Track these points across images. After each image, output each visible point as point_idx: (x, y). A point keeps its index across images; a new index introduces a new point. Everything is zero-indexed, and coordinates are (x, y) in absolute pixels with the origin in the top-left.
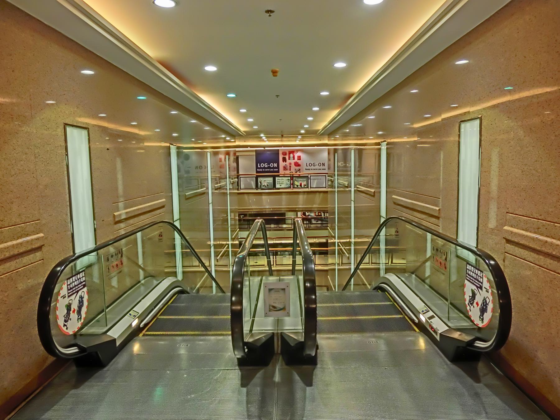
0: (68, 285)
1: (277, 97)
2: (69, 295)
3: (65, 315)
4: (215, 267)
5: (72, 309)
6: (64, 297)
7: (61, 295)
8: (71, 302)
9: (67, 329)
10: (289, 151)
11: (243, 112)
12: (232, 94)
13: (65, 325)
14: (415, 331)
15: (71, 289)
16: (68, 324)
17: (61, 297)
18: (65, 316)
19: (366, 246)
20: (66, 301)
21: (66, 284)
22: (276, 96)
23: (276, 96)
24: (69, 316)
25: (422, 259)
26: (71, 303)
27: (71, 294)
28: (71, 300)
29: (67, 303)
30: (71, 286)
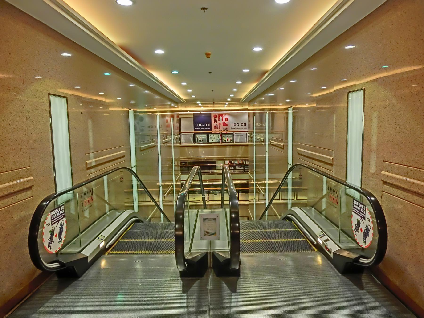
0: (51, 216)
1: (210, 74)
2: (52, 223)
3: (49, 238)
5: (55, 234)
6: (48, 225)
7: (46, 224)
8: (53, 228)
9: (51, 249)
10: (219, 115)
11: (184, 85)
12: (176, 71)
13: (49, 246)
15: (54, 218)
16: (52, 245)
17: (46, 225)
18: (49, 239)
20: (50, 228)
21: (50, 215)
22: (209, 73)
23: (209, 73)
24: (53, 240)
26: (54, 229)
27: (53, 222)
28: (54, 227)
29: (51, 229)
30: (54, 217)
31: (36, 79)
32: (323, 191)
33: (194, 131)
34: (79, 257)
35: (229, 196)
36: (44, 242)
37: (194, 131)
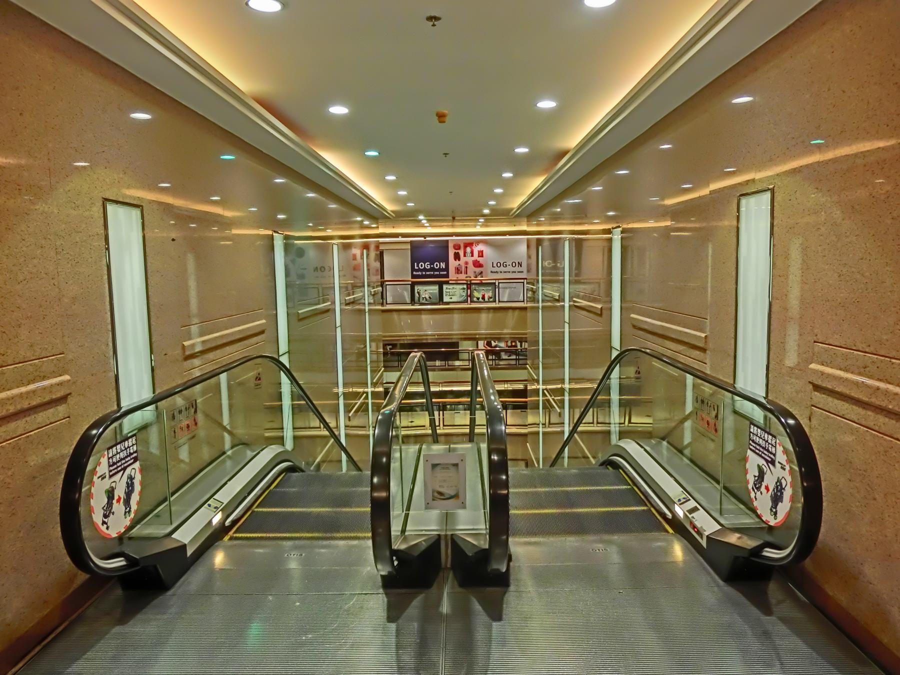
0: (109, 459)
1: (446, 156)
2: (111, 473)
3: (105, 506)
5: (116, 497)
6: (103, 477)
7: (98, 475)
8: (114, 485)
9: (107, 528)
12: (373, 151)
13: (104, 523)
15: (114, 464)
16: (110, 520)
17: (98, 478)
18: (105, 508)
19: (589, 395)
20: (107, 484)
21: (106, 457)
22: (444, 154)
23: (444, 154)
24: (112, 508)
26: (114, 487)
27: (113, 472)
28: (114, 482)
29: (107, 487)
30: (114, 460)
33: (412, 278)
35: (486, 416)
37: (412, 278)
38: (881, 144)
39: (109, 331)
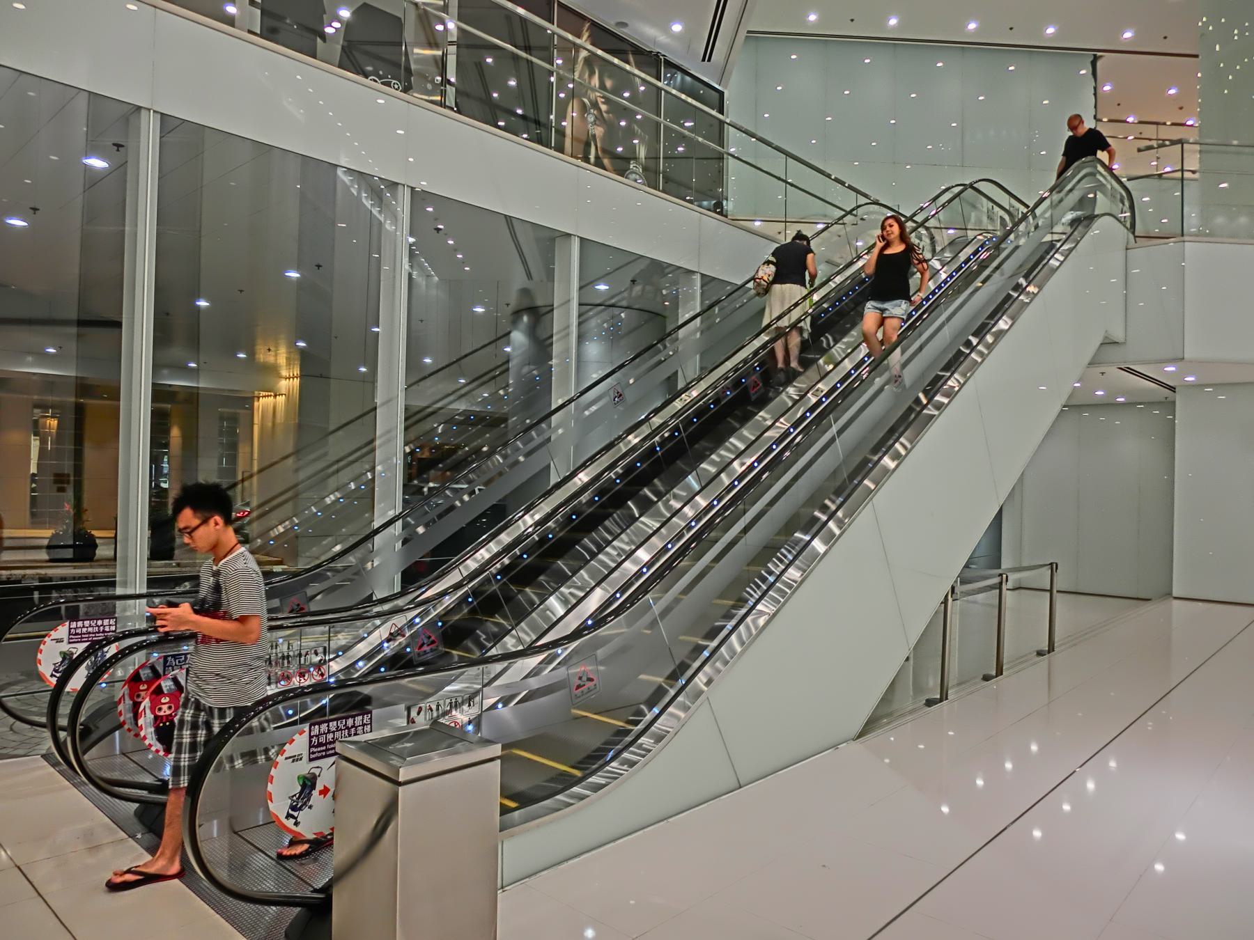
0: (311, 737)
1: (118, 150)
2: (312, 756)
3: (295, 795)
4: (115, 573)
5: (319, 787)
6: (296, 759)
7: (286, 755)
8: (317, 772)
9: (296, 824)
10: (1068, 225)
11: (689, 126)
12: (98, 159)
13: (289, 816)
14: (632, 716)
15: (320, 745)
16: (302, 815)
17: (286, 758)
18: (295, 798)
19: (796, 537)
20: (305, 768)
21: (307, 734)
22: (114, 145)
23: (114, 145)
24: (309, 800)
25: (232, 481)
26: (317, 774)
27: (317, 755)
28: (318, 767)
29: (305, 772)
30: (322, 739)
31: (1098, 230)
32: (809, 459)
33: (78, 606)
34: (198, 750)
35: (795, 587)
36: (39, 665)
37: (78, 606)
38: (733, 422)
39: (686, 693)
